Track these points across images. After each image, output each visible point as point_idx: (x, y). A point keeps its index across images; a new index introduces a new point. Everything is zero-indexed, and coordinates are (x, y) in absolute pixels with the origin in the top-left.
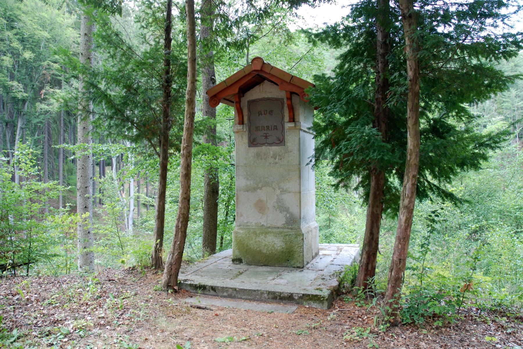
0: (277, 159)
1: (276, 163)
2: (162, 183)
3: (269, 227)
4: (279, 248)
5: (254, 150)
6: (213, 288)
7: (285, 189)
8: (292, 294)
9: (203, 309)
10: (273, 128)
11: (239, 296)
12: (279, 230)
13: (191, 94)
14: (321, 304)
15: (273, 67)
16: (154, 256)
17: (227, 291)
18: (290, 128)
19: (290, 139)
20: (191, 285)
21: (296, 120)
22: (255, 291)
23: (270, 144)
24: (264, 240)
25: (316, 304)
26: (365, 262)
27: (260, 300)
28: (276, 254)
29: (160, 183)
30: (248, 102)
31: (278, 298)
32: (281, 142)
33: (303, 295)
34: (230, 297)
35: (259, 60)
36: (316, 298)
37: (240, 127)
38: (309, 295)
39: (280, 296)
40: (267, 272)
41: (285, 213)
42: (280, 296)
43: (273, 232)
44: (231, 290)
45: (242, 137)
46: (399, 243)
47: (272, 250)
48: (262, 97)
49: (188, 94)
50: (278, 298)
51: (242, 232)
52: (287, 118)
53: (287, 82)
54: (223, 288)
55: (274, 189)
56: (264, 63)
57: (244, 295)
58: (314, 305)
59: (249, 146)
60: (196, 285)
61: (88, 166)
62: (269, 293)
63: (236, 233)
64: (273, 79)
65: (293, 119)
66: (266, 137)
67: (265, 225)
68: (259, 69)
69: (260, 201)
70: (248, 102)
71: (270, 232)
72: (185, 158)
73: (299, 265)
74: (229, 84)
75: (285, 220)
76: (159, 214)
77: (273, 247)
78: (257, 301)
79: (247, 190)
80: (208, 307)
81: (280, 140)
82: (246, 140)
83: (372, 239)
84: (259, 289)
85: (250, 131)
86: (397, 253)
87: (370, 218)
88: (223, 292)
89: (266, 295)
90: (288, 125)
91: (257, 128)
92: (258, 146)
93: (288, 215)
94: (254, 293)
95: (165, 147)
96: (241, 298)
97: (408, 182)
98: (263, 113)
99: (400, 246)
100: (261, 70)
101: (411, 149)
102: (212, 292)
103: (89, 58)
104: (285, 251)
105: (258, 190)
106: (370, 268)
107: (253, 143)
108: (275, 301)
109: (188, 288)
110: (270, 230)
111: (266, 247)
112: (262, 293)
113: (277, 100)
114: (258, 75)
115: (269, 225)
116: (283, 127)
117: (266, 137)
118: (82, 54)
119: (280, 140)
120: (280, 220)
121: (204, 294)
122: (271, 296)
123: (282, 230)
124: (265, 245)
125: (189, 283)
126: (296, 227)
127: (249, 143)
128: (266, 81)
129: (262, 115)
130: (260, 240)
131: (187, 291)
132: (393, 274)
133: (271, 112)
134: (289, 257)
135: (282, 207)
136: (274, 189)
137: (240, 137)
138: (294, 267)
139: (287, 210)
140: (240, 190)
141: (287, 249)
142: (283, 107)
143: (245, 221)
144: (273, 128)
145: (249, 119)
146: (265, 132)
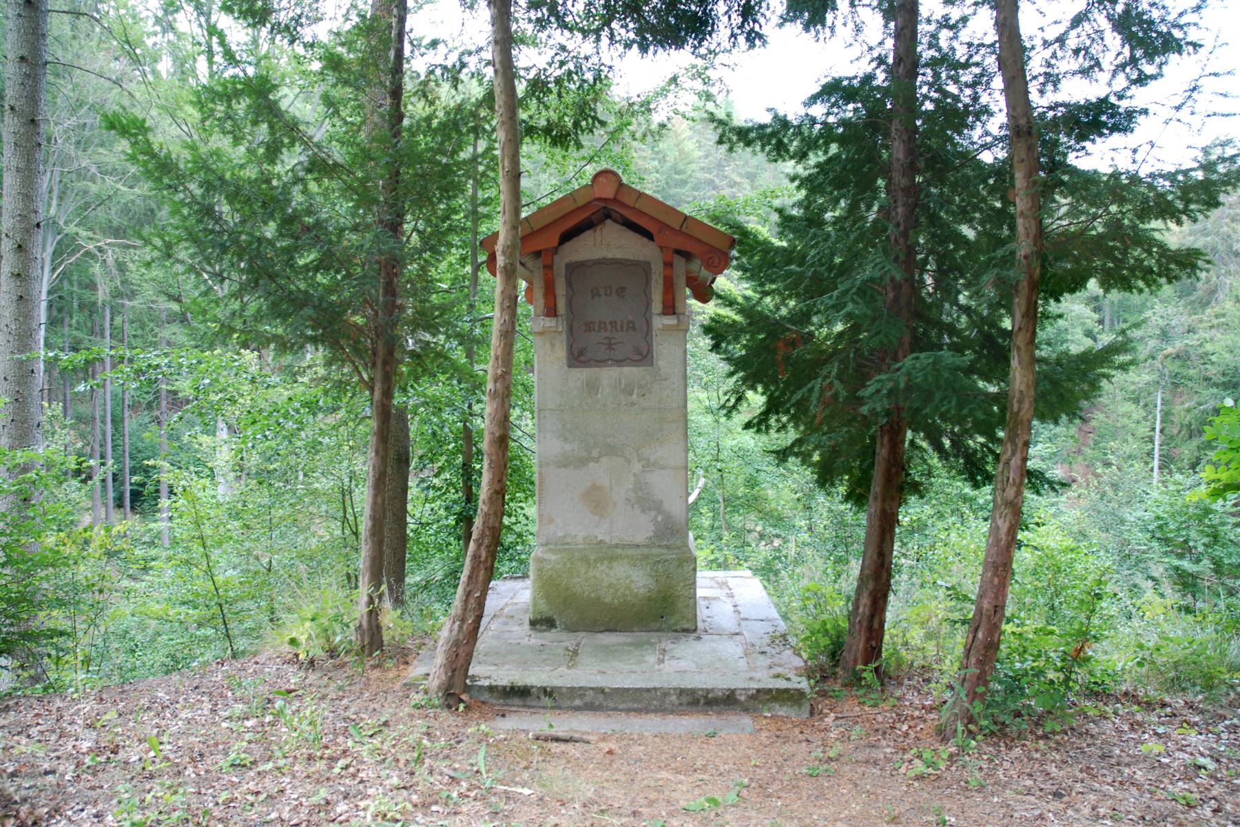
0: (635, 396)
1: (633, 404)
2: (381, 453)
3: (617, 546)
4: (642, 591)
5: (581, 375)
6: (548, 692)
7: (652, 460)
8: (733, 692)
9: (566, 741)
10: (625, 326)
11: (611, 705)
12: (639, 551)
13: (511, 255)
14: (796, 707)
15: (641, 195)
16: (365, 623)
17: (582, 696)
18: (667, 329)
19: (664, 350)
20: (491, 689)
21: (679, 310)
22: (648, 690)
23: (619, 362)
24: (607, 575)
25: (785, 708)
26: (867, 613)
27: (662, 710)
28: (633, 605)
29: (377, 452)
30: (567, 266)
31: (702, 701)
32: (644, 357)
33: (758, 691)
34: (591, 707)
35: (610, 176)
36: (786, 696)
37: (550, 323)
38: (770, 690)
39: (706, 697)
40: (626, 644)
41: (653, 513)
42: (706, 697)
43: (627, 556)
44: (591, 692)
45: (553, 345)
46: (995, 574)
47: (625, 595)
48: (613, 259)
49: (504, 252)
50: (702, 701)
51: (553, 558)
52: (657, 306)
53: (673, 229)
54: (572, 689)
55: (628, 461)
56: (621, 184)
57: (623, 702)
58: (782, 711)
59: (569, 366)
60: (504, 688)
61: (30, 395)
62: (682, 692)
63: (540, 561)
64: (641, 222)
65: (670, 308)
66: (610, 346)
67: (607, 540)
68: (611, 196)
69: (595, 488)
70: (567, 266)
71: (618, 557)
72: (498, 400)
73: (686, 626)
74: (536, 227)
75: (653, 528)
76: (374, 526)
77: (628, 588)
78: (655, 711)
79: (564, 462)
80: (576, 736)
81: (640, 354)
82: (561, 352)
83: (882, 565)
84: (658, 685)
85: (571, 331)
86: (991, 594)
87: (878, 523)
88: (572, 698)
89: (674, 698)
90: (659, 322)
91: (589, 327)
92: (590, 366)
93: (660, 518)
94: (645, 695)
95: (388, 368)
96: (616, 709)
97: (1013, 454)
98: (602, 292)
99: (996, 581)
100: (615, 200)
101: (1021, 392)
102: (547, 701)
103: (33, 121)
104: (654, 596)
105: (591, 464)
106: (876, 625)
107: (577, 358)
108: (694, 709)
109: (486, 696)
110: (619, 551)
111: (612, 591)
112: (666, 694)
113: (635, 264)
114: (605, 208)
115: (616, 541)
116: (649, 324)
117: (610, 346)
118: (12, 108)
119: (640, 354)
120: (640, 529)
121: (525, 706)
122: (685, 699)
123: (646, 551)
124: (610, 586)
125: (487, 683)
126: (678, 543)
127: (569, 359)
128: (608, 222)
129: (599, 295)
130: (598, 575)
131: (483, 703)
132: (980, 635)
133: (621, 291)
134: (664, 612)
135: (645, 501)
136: (628, 461)
137: (548, 345)
138: (676, 631)
139: (658, 507)
140: (548, 464)
141: (659, 592)
142: (648, 282)
143: (560, 534)
144: (625, 326)
145: (569, 305)
146: (607, 334)
